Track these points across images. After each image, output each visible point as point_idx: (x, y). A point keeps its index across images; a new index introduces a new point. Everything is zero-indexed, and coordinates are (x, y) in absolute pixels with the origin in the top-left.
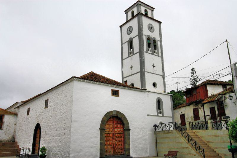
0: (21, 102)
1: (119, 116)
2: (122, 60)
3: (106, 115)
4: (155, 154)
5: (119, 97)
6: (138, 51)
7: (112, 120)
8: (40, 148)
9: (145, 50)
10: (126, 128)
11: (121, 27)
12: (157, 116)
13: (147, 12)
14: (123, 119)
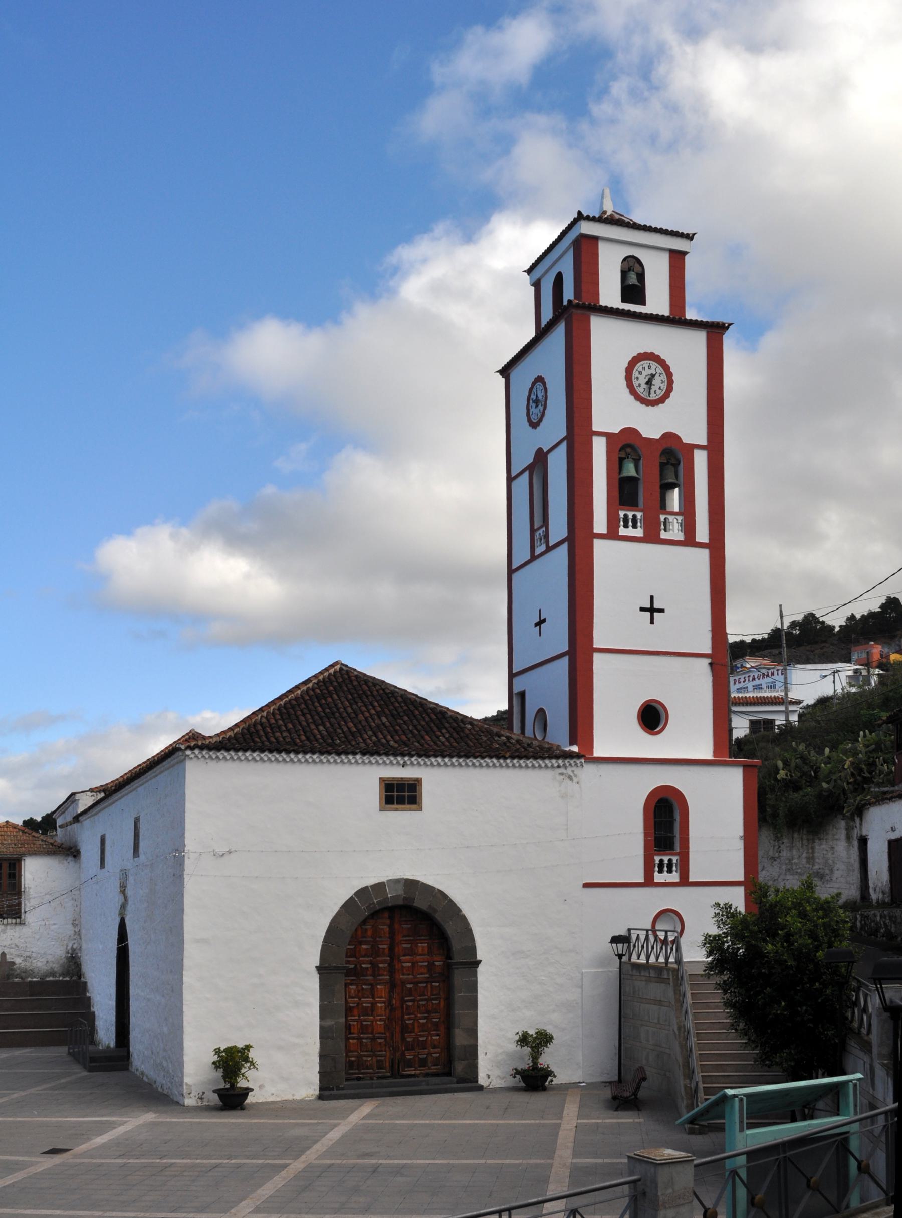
0: (91, 790)
1: (420, 903)
2: (511, 572)
3: (349, 906)
4: (616, 1078)
5: (422, 810)
6: (564, 534)
7: (388, 922)
8: (733, 739)
9: (600, 525)
10: (457, 958)
11: (505, 372)
12: (649, 882)
13: (641, 276)
14: (438, 917)
